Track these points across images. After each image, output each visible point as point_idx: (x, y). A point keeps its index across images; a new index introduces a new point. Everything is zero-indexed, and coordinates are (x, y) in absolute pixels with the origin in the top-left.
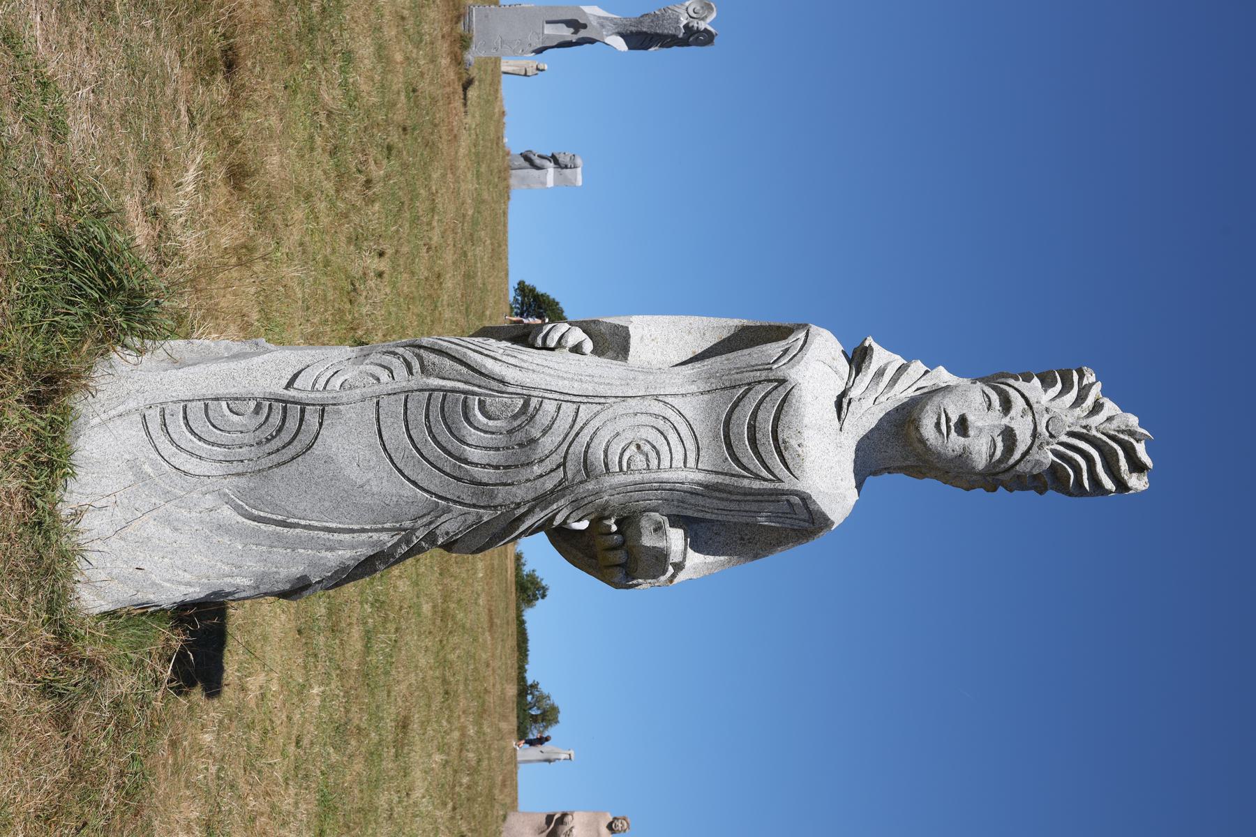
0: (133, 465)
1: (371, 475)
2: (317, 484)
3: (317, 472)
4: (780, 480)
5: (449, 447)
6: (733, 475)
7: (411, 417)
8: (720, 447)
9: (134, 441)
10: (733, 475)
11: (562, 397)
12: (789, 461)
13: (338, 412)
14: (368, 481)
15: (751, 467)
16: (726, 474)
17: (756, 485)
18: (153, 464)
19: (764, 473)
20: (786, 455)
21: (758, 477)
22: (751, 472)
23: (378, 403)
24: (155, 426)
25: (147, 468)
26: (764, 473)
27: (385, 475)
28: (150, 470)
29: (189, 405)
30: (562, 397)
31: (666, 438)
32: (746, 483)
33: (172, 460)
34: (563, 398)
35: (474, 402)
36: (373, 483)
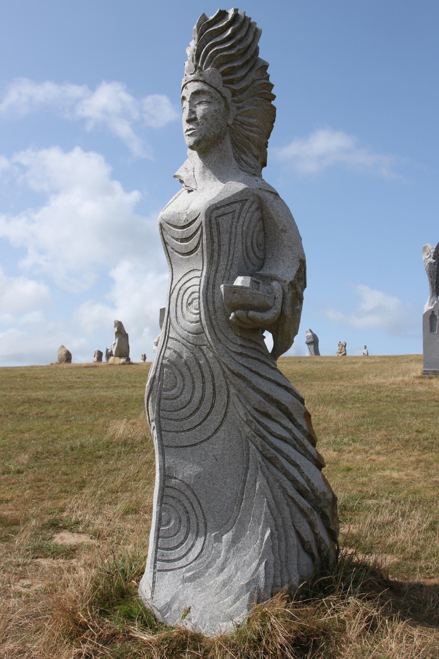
0: (185, 580)
1: (210, 454)
2: (214, 484)
3: (206, 484)
4: (201, 223)
5: (193, 409)
6: (203, 250)
7: (220, 417)
8: (192, 258)
9: (171, 579)
10: (203, 250)
11: (165, 346)
12: (193, 219)
13: (169, 468)
14: (214, 456)
15: (197, 239)
16: (203, 254)
17: (204, 237)
18: (188, 571)
19: (199, 232)
20: (190, 220)
21: (201, 235)
22: (200, 239)
23: (166, 446)
24: (168, 566)
25: (188, 575)
26: (199, 232)
27: (211, 446)
28: (190, 573)
29: (159, 546)
30: (165, 346)
31: (190, 287)
32: (204, 242)
33: (190, 560)
34: (165, 346)
35: (165, 394)
36: (215, 453)
